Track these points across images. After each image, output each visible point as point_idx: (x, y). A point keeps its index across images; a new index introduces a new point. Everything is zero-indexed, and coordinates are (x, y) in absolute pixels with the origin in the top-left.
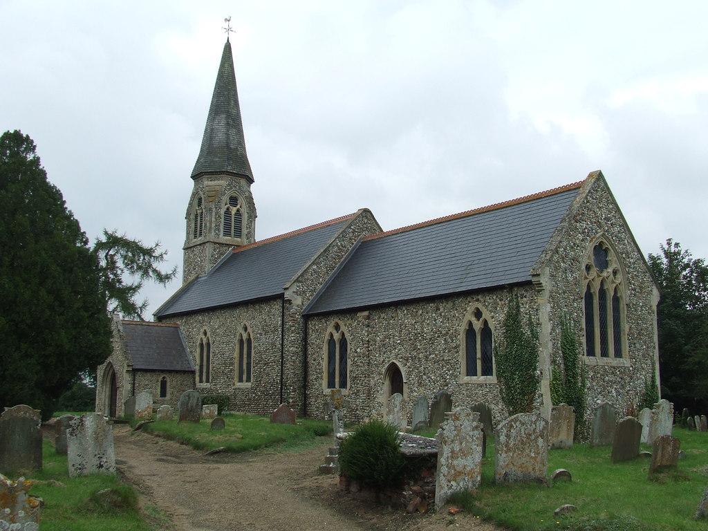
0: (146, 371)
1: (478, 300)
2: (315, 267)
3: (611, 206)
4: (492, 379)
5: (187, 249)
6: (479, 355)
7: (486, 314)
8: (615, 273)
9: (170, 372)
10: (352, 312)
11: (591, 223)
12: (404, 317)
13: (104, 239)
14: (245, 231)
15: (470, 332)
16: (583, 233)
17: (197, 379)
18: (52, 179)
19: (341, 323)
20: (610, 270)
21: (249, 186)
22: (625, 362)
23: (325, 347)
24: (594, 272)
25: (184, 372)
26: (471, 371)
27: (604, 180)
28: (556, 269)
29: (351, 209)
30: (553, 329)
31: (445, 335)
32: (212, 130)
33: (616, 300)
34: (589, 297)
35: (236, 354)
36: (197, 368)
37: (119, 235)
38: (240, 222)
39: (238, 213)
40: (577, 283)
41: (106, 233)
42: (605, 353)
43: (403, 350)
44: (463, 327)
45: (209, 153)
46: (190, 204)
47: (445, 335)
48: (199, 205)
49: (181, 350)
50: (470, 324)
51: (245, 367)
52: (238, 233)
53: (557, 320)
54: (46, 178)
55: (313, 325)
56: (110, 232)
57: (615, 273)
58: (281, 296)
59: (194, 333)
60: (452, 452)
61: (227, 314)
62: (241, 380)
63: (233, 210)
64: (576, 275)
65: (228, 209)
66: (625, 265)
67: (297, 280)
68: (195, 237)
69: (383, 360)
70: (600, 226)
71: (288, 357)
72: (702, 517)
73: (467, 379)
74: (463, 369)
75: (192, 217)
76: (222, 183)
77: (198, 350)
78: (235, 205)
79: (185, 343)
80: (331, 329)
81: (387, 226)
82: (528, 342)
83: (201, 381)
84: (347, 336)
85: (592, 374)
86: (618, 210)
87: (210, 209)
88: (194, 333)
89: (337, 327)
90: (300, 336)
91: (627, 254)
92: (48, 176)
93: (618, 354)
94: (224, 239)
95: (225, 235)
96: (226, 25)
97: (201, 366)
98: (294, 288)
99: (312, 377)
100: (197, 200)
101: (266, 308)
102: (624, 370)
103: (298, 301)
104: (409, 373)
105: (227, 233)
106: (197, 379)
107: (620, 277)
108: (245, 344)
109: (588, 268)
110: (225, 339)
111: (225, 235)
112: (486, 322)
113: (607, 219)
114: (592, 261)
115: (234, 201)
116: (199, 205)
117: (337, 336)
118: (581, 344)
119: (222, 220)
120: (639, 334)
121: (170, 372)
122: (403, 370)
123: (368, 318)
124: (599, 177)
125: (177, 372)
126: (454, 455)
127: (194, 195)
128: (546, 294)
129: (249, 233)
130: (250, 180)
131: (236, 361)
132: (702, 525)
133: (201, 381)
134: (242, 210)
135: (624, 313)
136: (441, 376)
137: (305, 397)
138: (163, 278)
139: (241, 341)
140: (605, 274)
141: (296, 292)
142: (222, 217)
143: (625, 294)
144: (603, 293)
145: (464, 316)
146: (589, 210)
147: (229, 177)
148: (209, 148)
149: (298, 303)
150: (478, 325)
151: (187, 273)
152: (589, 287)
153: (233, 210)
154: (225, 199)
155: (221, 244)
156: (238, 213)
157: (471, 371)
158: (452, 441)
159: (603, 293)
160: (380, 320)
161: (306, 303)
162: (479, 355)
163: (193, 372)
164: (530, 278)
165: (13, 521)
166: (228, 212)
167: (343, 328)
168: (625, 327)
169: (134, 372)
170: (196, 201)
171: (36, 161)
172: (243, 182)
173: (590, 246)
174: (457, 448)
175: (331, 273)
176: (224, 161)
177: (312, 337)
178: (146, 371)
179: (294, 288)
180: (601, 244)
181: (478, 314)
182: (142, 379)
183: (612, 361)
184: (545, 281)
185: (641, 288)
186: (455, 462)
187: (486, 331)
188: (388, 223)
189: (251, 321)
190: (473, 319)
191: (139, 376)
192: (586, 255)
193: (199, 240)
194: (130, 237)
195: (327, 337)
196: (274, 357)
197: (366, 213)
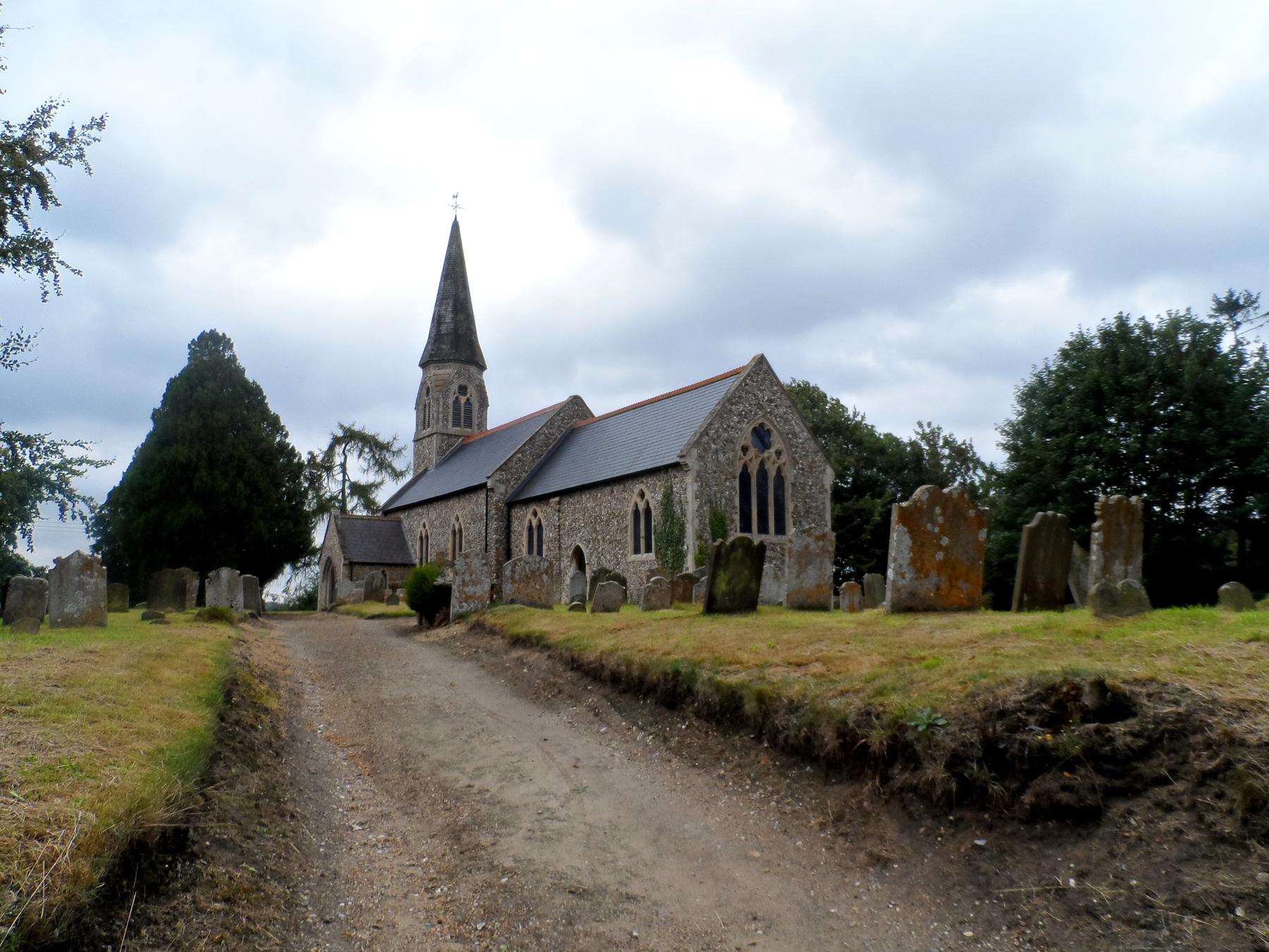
0: (365, 564)
4: (652, 556)
5: (416, 441)
7: (648, 496)
8: (779, 453)
9: (389, 565)
10: (544, 498)
12: (587, 500)
13: (340, 433)
14: (475, 421)
15: (636, 513)
16: (740, 414)
18: (250, 376)
19: (538, 510)
20: (772, 450)
23: (525, 534)
24: (752, 452)
25: (405, 565)
28: (705, 450)
30: (700, 507)
33: (780, 479)
34: (745, 477)
35: (450, 546)
36: (417, 561)
37: (356, 428)
38: (471, 411)
40: (731, 463)
41: (342, 426)
43: (585, 533)
44: (630, 509)
45: (436, 341)
46: (419, 394)
49: (403, 546)
50: (636, 505)
52: (469, 423)
53: (705, 498)
55: (517, 512)
56: (347, 425)
57: (779, 453)
58: (483, 486)
59: (414, 525)
60: (463, 581)
63: (463, 399)
64: (730, 455)
66: (792, 446)
67: (500, 469)
69: (570, 543)
70: (760, 407)
71: (492, 545)
73: (634, 557)
74: (630, 547)
75: (421, 407)
76: (448, 371)
78: (465, 394)
79: (408, 537)
80: (529, 516)
82: (678, 519)
84: (544, 523)
87: (438, 399)
88: (414, 525)
89: (535, 514)
90: (503, 524)
94: (452, 430)
95: (454, 425)
96: (453, 202)
100: (425, 389)
101: (474, 497)
104: (591, 555)
105: (456, 423)
107: (784, 458)
108: (457, 534)
109: (745, 449)
110: (441, 530)
111: (454, 425)
112: (648, 503)
113: (770, 401)
114: (749, 442)
115: (463, 390)
117: (534, 523)
118: (733, 521)
119: (451, 410)
120: (807, 512)
121: (389, 565)
122: (586, 552)
123: (559, 503)
124: (761, 360)
125: (397, 565)
126: (464, 583)
127: (423, 384)
130: (482, 367)
131: (450, 552)
134: (472, 400)
136: (615, 556)
138: (397, 475)
139: (454, 532)
140: (766, 455)
141: (499, 481)
143: (790, 474)
144: (763, 473)
145: (630, 498)
146: (748, 392)
147: (458, 365)
148: (437, 336)
149: (501, 492)
150: (642, 506)
151: (417, 466)
152: (745, 467)
153: (463, 399)
154: (455, 388)
155: (449, 435)
157: (637, 550)
159: (763, 473)
160: (569, 504)
161: (510, 491)
164: (678, 460)
165: (91, 577)
166: (457, 401)
167: (540, 514)
168: (790, 506)
170: (425, 391)
171: (233, 359)
172: (473, 369)
173: (747, 428)
174: (467, 578)
175: (537, 461)
176: (454, 339)
177: (515, 525)
178: (365, 564)
180: (762, 425)
181: (642, 495)
184: (692, 462)
185: (811, 468)
186: (466, 589)
187: (648, 511)
188: (598, 406)
189: (462, 512)
190: (639, 500)
192: (745, 435)
194: (369, 431)
195: (526, 524)
196: (479, 547)
197: (576, 401)
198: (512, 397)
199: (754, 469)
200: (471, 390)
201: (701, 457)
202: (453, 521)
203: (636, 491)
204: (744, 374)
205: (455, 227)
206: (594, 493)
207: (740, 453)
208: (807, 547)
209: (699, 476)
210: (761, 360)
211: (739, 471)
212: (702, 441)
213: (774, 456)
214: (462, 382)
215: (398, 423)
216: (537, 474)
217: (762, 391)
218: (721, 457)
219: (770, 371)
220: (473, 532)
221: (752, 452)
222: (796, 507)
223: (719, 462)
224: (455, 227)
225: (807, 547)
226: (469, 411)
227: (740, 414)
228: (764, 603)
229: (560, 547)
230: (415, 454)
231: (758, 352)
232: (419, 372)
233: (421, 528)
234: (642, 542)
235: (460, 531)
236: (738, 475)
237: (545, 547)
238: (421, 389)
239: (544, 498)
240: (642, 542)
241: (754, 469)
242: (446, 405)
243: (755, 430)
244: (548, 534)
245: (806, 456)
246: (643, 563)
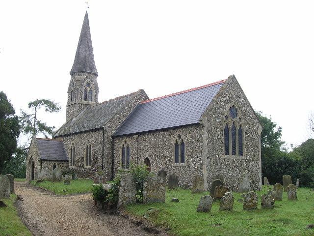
5: (68, 106)
7: (182, 137)
10: (132, 135)
15: (177, 144)
16: (224, 102)
17: (70, 164)
20: (238, 118)
21: (96, 78)
22: (244, 157)
23: (121, 150)
26: (177, 161)
27: (236, 79)
29: (225, 77)
30: (208, 143)
31: (167, 146)
32: (79, 53)
33: (241, 131)
35: (85, 153)
36: (70, 159)
39: (91, 90)
42: (234, 154)
44: (173, 143)
46: (69, 86)
47: (167, 146)
48: (73, 86)
51: (88, 159)
52: (90, 99)
55: (116, 141)
57: (240, 119)
60: (124, 190)
61: (81, 136)
62: (87, 165)
63: (88, 89)
65: (86, 88)
71: (105, 154)
72: (311, 227)
74: (173, 158)
75: (70, 92)
77: (70, 152)
80: (123, 143)
81: (151, 97)
83: (71, 165)
84: (130, 145)
86: (242, 91)
89: (126, 142)
91: (247, 111)
93: (241, 154)
97: (71, 159)
98: (108, 125)
99: (116, 163)
100: (72, 84)
102: (243, 161)
103: (109, 130)
106: (70, 164)
107: (242, 121)
108: (89, 149)
109: (227, 117)
113: (237, 96)
115: (88, 85)
116: (73, 86)
122: (151, 161)
126: (124, 191)
127: (71, 81)
128: (206, 128)
130: (97, 75)
132: (311, 231)
133: (71, 165)
134: (92, 89)
135: (244, 136)
137: (113, 172)
140: (235, 120)
142: (83, 92)
143: (245, 128)
145: (173, 138)
149: (111, 132)
150: (179, 142)
153: (88, 89)
154: (85, 84)
156: (91, 90)
160: (143, 139)
163: (68, 161)
164: (199, 122)
167: (128, 142)
169: (41, 161)
172: (93, 76)
173: (228, 107)
176: (84, 67)
177: (116, 145)
178: (47, 160)
179: (108, 125)
180: (233, 106)
181: (180, 137)
182: (44, 164)
183: (237, 157)
188: (151, 96)
191: (43, 162)
193: (74, 102)
197: (142, 92)
199: (230, 126)
201: (209, 121)
202: (87, 143)
205: (86, 16)
207: (225, 119)
209: (209, 130)
210: (233, 78)
211: (224, 126)
212: (207, 113)
213: (238, 120)
215: (62, 99)
216: (125, 124)
219: (237, 82)
220: (97, 149)
221: (230, 119)
223: (216, 123)
224: (86, 16)
226: (90, 94)
227: (224, 102)
228: (275, 207)
230: (68, 112)
231: (231, 74)
232: (70, 77)
233: (71, 145)
234: (179, 158)
237: (130, 157)
238: (70, 83)
240: (179, 158)
241: (230, 126)
242: (81, 92)
244: (132, 151)
246: (180, 167)
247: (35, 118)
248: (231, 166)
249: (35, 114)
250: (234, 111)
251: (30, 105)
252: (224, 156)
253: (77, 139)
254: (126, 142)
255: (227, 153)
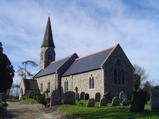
1: (92, 72)
2: (63, 66)
3: (121, 51)
6: (92, 84)
7: (93, 75)
11: (116, 55)
15: (90, 79)
16: (114, 57)
20: (121, 65)
23: (64, 83)
26: (90, 88)
30: (106, 78)
42: (119, 83)
44: (89, 78)
50: (90, 77)
54: (2, 51)
57: (122, 66)
60: (54, 97)
68: (42, 60)
69: (75, 86)
70: (118, 55)
74: (89, 87)
79: (38, 84)
85: (116, 88)
89: (66, 79)
92: (3, 50)
93: (123, 83)
105: (49, 59)
108: (49, 84)
109: (115, 65)
112: (93, 77)
115: (50, 52)
129: (53, 59)
130: (55, 47)
139: (48, 83)
150: (91, 78)
153: (50, 54)
154: (48, 51)
157: (90, 88)
158: (54, 95)
162: (92, 84)
166: (49, 55)
167: (68, 79)
170: (42, 53)
172: (52, 48)
174: (55, 97)
176: (49, 43)
177: (62, 82)
180: (119, 59)
181: (91, 75)
186: (54, 99)
190: (91, 76)
198: (62, 54)
200: (52, 51)
202: (48, 80)
203: (90, 74)
204: (113, 49)
205: (49, 18)
206: (80, 74)
207: (114, 66)
208: (156, 92)
211: (114, 70)
213: (121, 67)
214: (50, 50)
217: (119, 52)
218: (110, 67)
222: (126, 78)
223: (110, 68)
224: (49, 18)
225: (156, 92)
229: (72, 87)
235: (50, 83)
236: (114, 71)
237: (69, 87)
239: (69, 76)
243: (117, 60)
244: (70, 84)
245: (128, 66)
247: (26, 70)
248: (118, 90)
249: (26, 68)
250: (119, 62)
251: (23, 63)
252: (114, 85)
253: (44, 79)
254: (66, 79)
255: (116, 83)
